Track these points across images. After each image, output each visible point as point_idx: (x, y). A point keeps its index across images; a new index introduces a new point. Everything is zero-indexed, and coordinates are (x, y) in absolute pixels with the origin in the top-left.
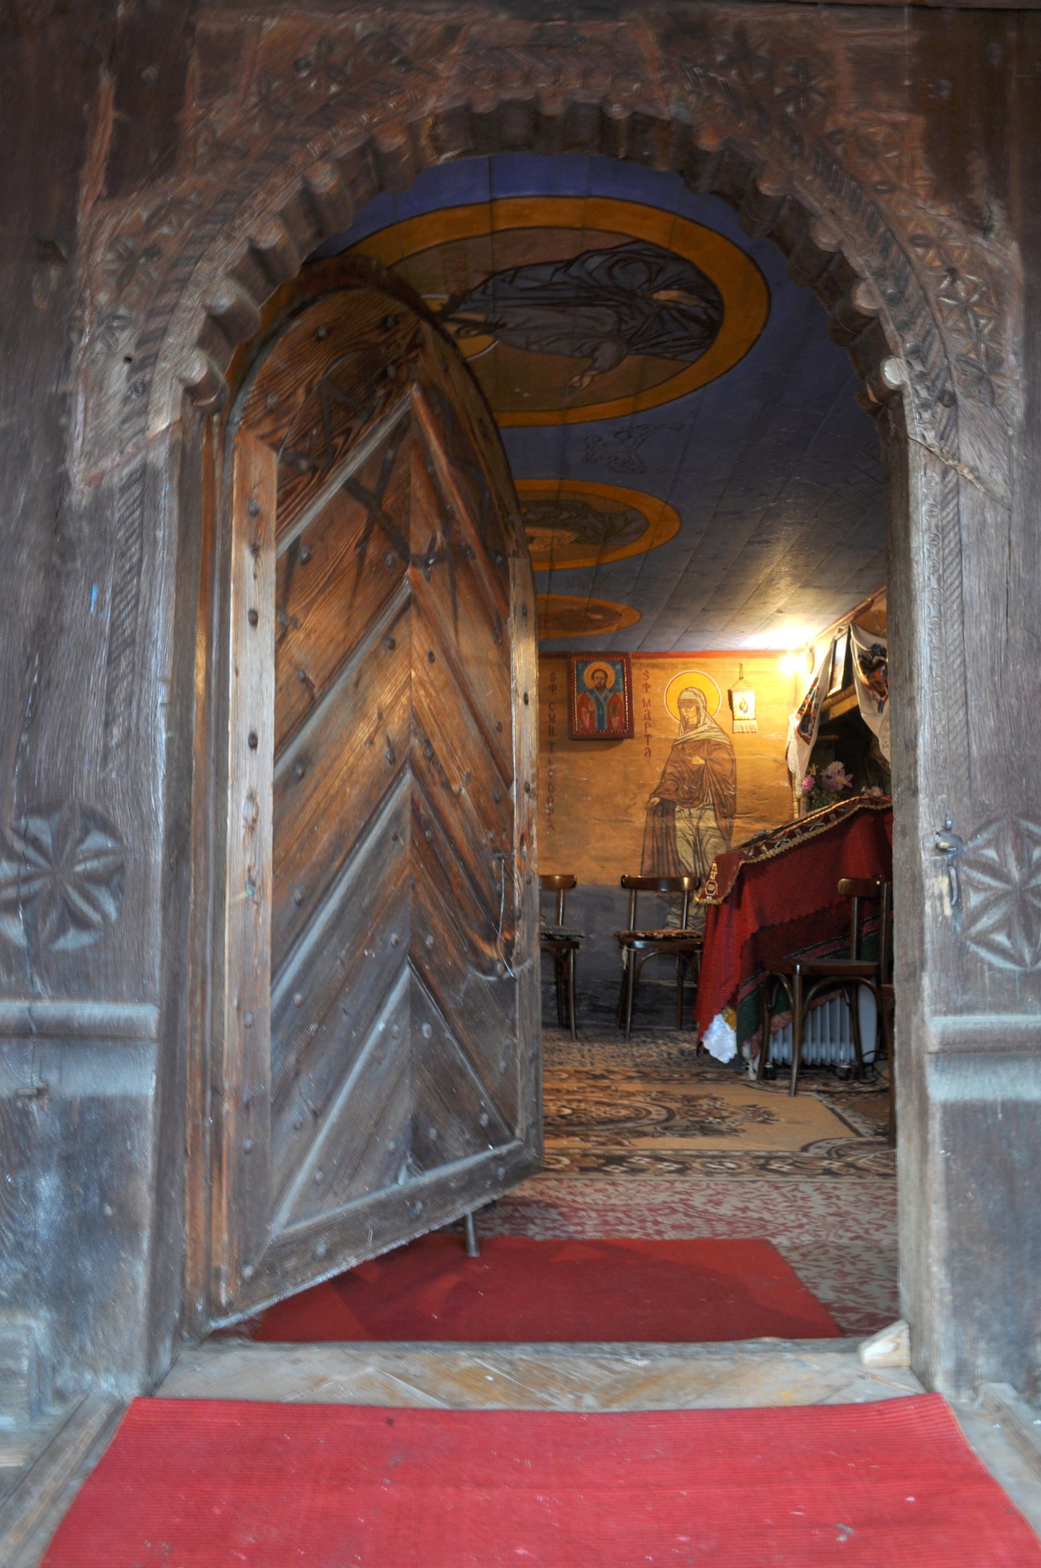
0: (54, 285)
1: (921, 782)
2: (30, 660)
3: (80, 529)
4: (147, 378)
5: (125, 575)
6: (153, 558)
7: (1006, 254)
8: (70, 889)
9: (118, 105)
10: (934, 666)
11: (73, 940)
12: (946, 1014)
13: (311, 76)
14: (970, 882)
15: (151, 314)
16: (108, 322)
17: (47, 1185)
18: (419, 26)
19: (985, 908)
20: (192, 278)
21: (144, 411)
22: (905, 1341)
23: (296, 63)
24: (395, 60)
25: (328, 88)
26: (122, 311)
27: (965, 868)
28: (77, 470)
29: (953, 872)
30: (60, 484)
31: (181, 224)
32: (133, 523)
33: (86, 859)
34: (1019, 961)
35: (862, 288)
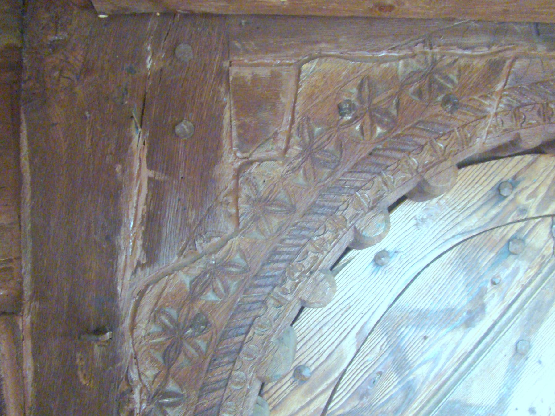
0: (98, 363)
13: (355, 118)
18: (462, 62)
20: (245, 348)
23: (339, 108)
25: (373, 131)
26: (172, 387)
31: (227, 289)
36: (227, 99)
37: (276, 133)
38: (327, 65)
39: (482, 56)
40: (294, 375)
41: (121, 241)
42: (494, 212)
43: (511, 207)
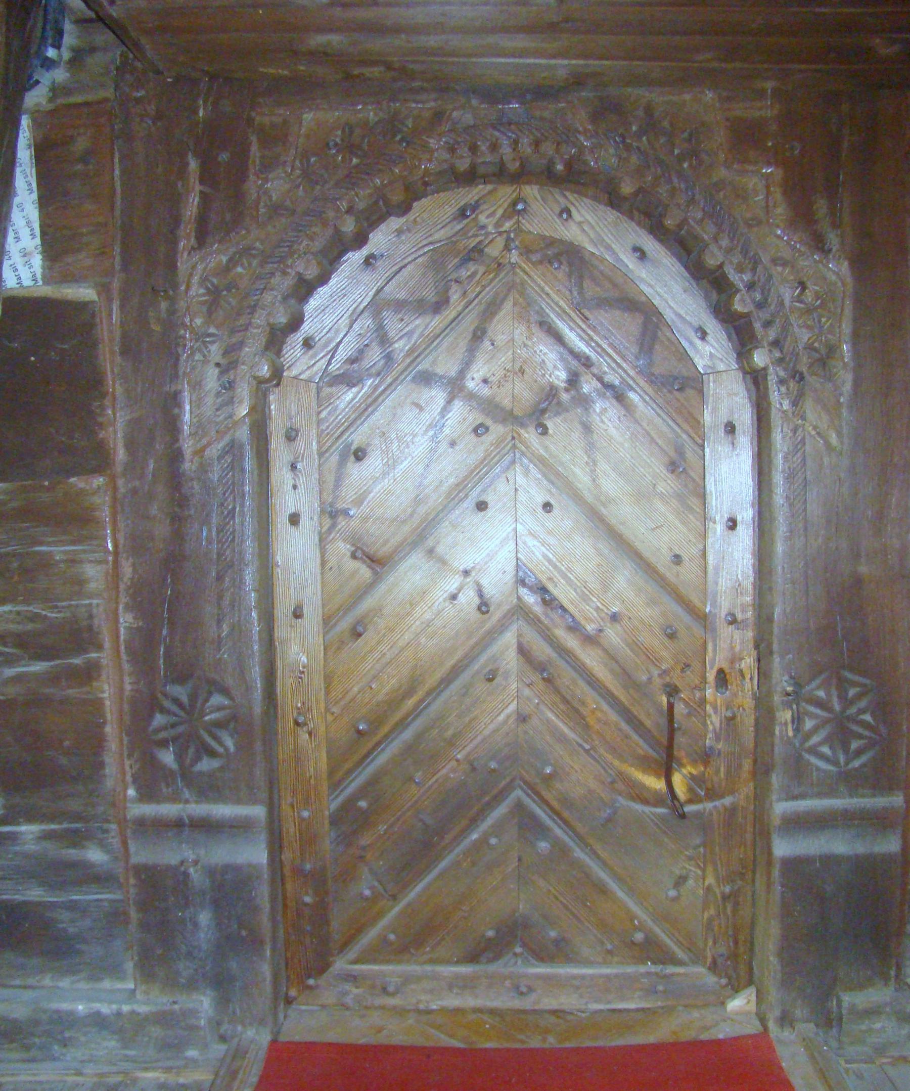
0: (164, 315)
1: (775, 647)
2: (165, 580)
3: (192, 488)
4: (232, 377)
5: (225, 518)
6: (242, 505)
7: (837, 270)
8: (202, 732)
9: (202, 182)
10: (785, 566)
11: (206, 765)
12: (786, 800)
14: (807, 713)
15: (233, 331)
16: (202, 337)
17: (205, 917)
18: (415, 112)
19: (815, 730)
21: (231, 401)
22: (754, 998)
23: (328, 144)
24: (399, 137)
25: (351, 160)
26: (212, 330)
27: (803, 704)
28: (188, 446)
29: (794, 707)
30: (176, 456)
31: (250, 265)
32: (227, 482)
33: (211, 712)
34: (836, 763)
35: (738, 297)
36: (254, 139)
37: (285, 162)
38: (321, 115)
39: (430, 109)
40: (303, 345)
42: (459, 227)
43: (473, 224)
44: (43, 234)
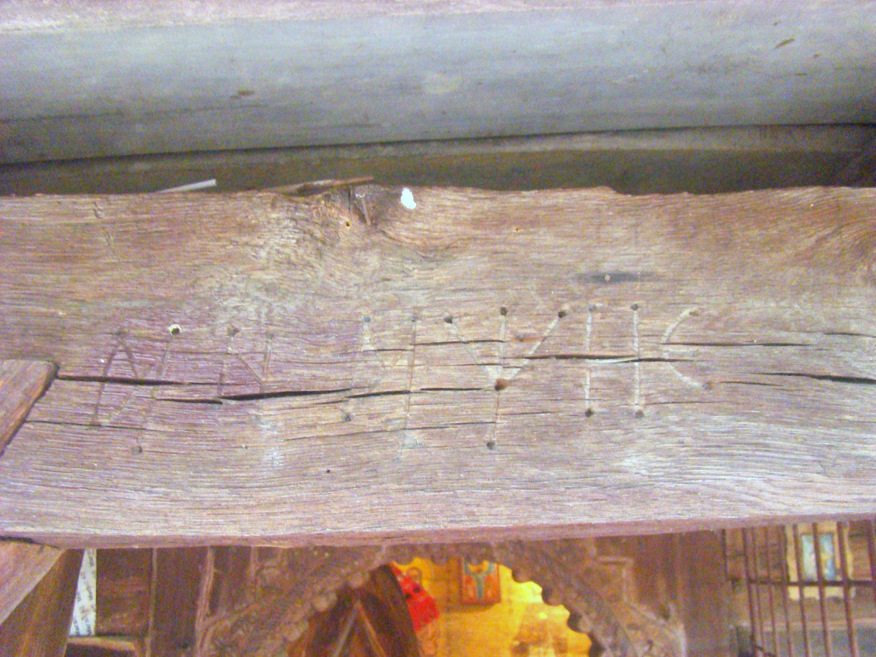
9: (216, 566)
41: (199, 603)
44: (98, 595)
